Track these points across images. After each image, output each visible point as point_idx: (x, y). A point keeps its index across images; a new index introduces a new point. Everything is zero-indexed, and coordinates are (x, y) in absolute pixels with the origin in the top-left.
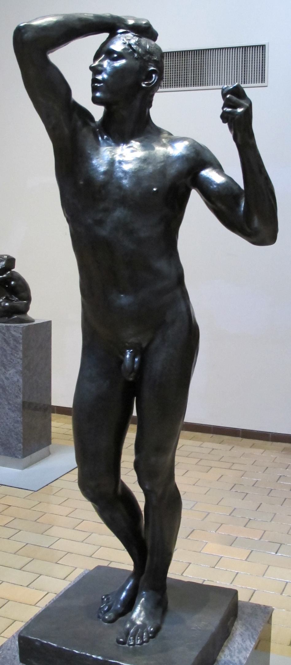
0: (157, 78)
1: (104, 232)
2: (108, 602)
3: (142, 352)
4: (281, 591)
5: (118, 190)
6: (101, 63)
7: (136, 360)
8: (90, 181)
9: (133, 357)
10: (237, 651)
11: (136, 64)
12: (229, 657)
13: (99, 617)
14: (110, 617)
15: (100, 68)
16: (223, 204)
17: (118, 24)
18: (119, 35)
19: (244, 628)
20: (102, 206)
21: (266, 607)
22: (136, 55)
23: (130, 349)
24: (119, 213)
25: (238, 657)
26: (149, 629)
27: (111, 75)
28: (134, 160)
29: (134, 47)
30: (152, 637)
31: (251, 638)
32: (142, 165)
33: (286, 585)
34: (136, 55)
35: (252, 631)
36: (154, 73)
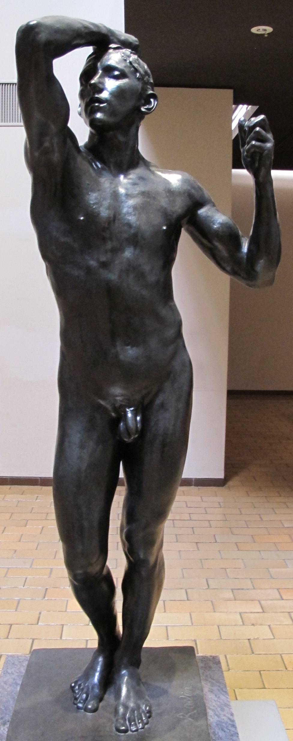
0: (156, 103)
1: (113, 276)
2: (83, 689)
3: (144, 409)
4: (166, 636)
5: (126, 228)
6: (101, 80)
7: (138, 418)
8: (92, 217)
9: (135, 414)
10: (219, 709)
11: (138, 85)
12: (216, 717)
13: (78, 708)
14: (93, 705)
15: (101, 86)
16: (219, 246)
17: (111, 38)
18: (111, 51)
19: (209, 684)
20: (109, 245)
21: (214, 658)
22: (138, 75)
23: (129, 407)
24: (128, 253)
25: (224, 715)
26: (144, 708)
27: (112, 94)
28: (138, 194)
29: (136, 65)
30: (149, 717)
31: (223, 693)
32: (145, 199)
33: (167, 630)
34: (138, 75)
35: (218, 684)
36: (152, 98)
